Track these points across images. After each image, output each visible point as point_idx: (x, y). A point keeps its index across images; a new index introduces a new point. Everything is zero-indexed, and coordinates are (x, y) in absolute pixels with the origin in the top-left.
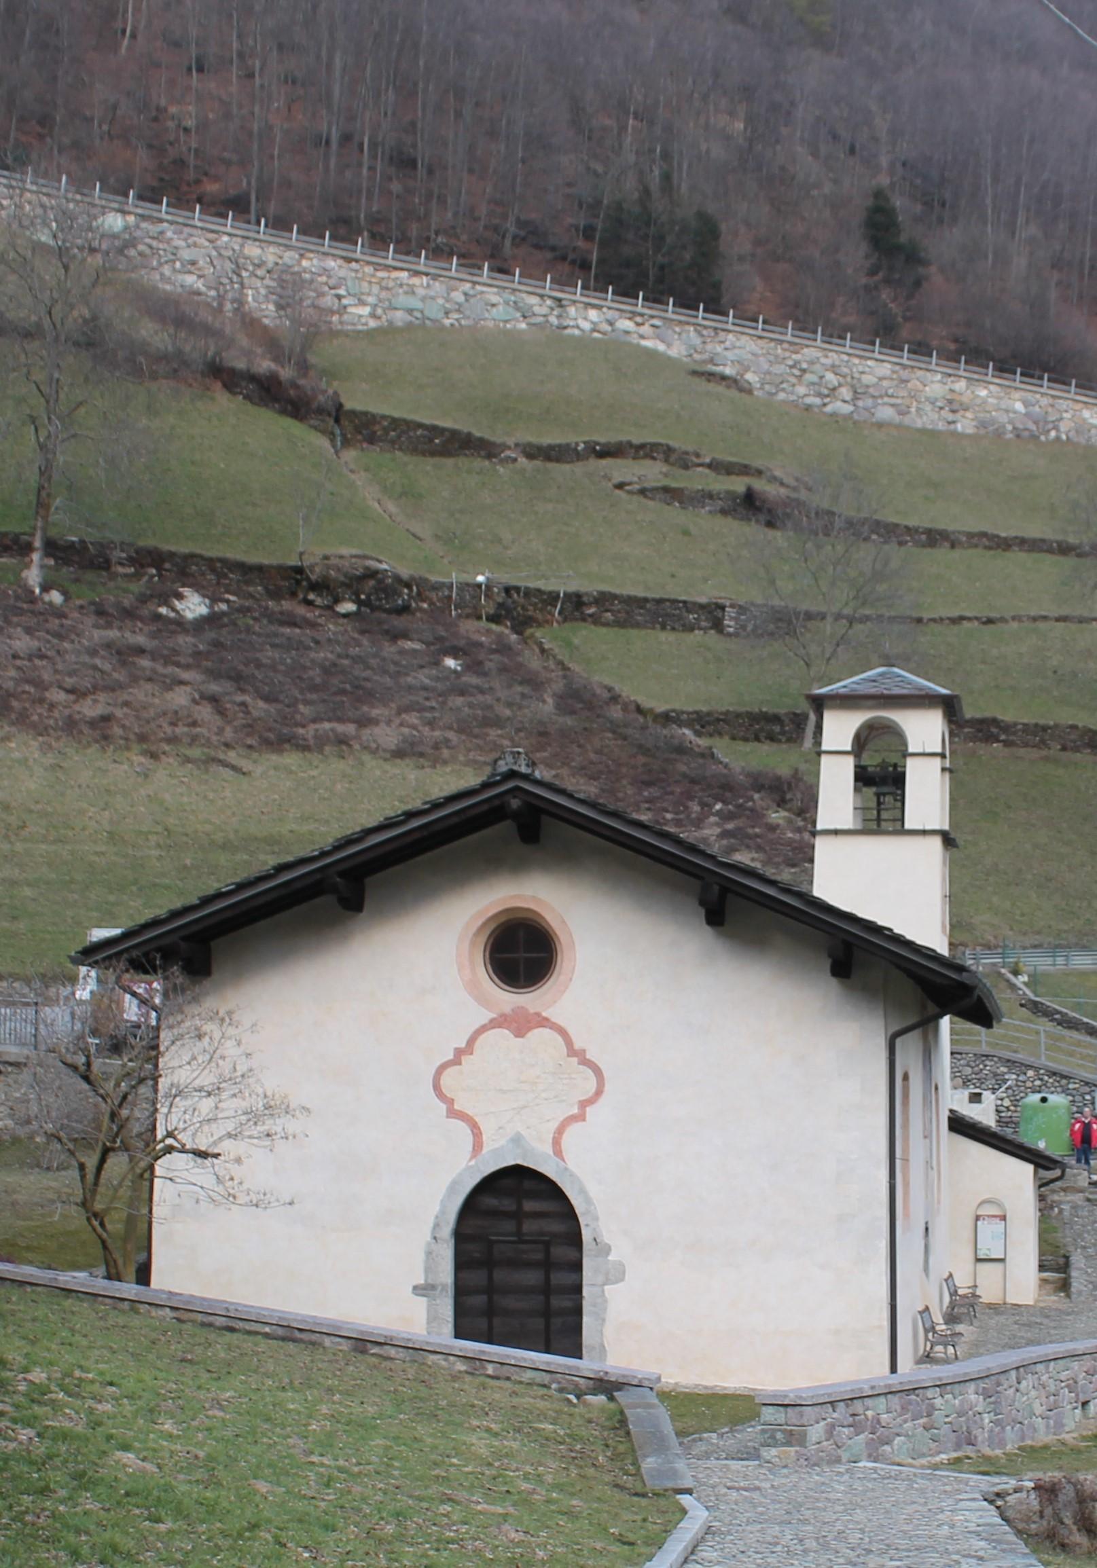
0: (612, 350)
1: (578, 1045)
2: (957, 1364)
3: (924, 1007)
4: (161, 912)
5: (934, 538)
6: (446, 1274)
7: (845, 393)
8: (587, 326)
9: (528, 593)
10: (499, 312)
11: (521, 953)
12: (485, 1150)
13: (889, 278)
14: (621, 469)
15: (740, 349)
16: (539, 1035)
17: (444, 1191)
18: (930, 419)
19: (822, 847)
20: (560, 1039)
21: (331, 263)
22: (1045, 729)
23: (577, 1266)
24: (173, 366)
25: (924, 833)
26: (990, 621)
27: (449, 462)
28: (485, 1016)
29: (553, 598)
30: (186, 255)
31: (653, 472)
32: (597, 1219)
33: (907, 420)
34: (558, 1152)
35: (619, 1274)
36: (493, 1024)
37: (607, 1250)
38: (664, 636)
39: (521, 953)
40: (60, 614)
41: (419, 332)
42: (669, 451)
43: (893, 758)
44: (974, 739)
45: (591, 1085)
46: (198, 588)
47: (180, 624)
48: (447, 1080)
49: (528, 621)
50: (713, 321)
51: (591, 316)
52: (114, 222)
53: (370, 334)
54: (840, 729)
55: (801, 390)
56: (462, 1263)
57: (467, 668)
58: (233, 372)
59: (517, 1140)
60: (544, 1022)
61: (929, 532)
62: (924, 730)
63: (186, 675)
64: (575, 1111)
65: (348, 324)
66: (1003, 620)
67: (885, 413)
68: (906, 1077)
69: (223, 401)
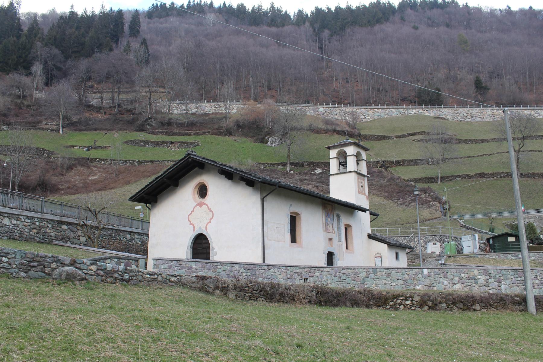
0: (417, 117)
4: (140, 189)
5: (483, 141)
7: (469, 117)
8: (413, 113)
9: (388, 162)
10: (395, 113)
13: (481, 93)
14: (414, 137)
15: (445, 112)
16: (204, 206)
18: (489, 119)
19: (331, 179)
21: (362, 110)
22: (496, 173)
24: (326, 131)
25: (351, 172)
26: (490, 155)
27: (381, 141)
29: (393, 162)
30: (335, 113)
31: (421, 137)
33: (483, 120)
34: (206, 230)
38: (416, 166)
39: (203, 191)
40: (292, 175)
41: (380, 119)
42: (425, 132)
44: (479, 177)
46: (319, 168)
47: (315, 174)
49: (388, 167)
50: (439, 107)
51: (413, 111)
52: (321, 109)
53: (370, 121)
55: (459, 118)
57: (371, 176)
58: (338, 131)
61: (482, 140)
63: (312, 183)
66: (493, 154)
67: (478, 119)
69: (336, 136)
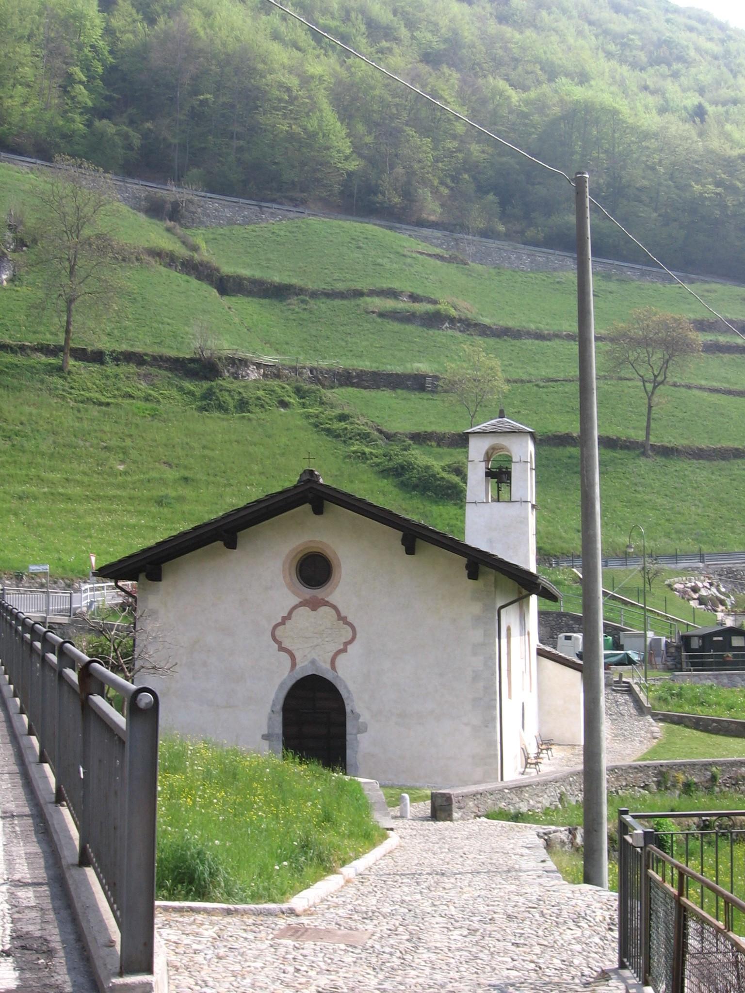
1: (343, 614)
2: (269, 711)
3: (520, 593)
6: (279, 730)
11: (314, 570)
12: (298, 667)
17: (277, 687)
20: (334, 612)
23: (343, 725)
28: (296, 600)
32: (353, 701)
35: (363, 729)
36: (301, 604)
37: (358, 716)
39: (314, 570)
43: (505, 464)
45: (350, 635)
48: (278, 633)
54: (477, 449)
56: (342, 736)
59: (313, 662)
60: (327, 604)
62: (525, 451)
64: (342, 647)
65: (49, 183)
68: (509, 629)
